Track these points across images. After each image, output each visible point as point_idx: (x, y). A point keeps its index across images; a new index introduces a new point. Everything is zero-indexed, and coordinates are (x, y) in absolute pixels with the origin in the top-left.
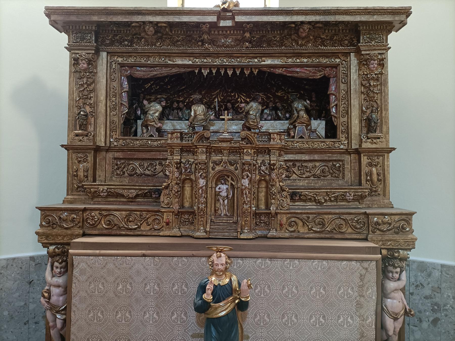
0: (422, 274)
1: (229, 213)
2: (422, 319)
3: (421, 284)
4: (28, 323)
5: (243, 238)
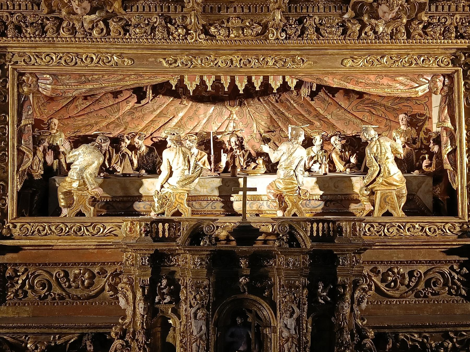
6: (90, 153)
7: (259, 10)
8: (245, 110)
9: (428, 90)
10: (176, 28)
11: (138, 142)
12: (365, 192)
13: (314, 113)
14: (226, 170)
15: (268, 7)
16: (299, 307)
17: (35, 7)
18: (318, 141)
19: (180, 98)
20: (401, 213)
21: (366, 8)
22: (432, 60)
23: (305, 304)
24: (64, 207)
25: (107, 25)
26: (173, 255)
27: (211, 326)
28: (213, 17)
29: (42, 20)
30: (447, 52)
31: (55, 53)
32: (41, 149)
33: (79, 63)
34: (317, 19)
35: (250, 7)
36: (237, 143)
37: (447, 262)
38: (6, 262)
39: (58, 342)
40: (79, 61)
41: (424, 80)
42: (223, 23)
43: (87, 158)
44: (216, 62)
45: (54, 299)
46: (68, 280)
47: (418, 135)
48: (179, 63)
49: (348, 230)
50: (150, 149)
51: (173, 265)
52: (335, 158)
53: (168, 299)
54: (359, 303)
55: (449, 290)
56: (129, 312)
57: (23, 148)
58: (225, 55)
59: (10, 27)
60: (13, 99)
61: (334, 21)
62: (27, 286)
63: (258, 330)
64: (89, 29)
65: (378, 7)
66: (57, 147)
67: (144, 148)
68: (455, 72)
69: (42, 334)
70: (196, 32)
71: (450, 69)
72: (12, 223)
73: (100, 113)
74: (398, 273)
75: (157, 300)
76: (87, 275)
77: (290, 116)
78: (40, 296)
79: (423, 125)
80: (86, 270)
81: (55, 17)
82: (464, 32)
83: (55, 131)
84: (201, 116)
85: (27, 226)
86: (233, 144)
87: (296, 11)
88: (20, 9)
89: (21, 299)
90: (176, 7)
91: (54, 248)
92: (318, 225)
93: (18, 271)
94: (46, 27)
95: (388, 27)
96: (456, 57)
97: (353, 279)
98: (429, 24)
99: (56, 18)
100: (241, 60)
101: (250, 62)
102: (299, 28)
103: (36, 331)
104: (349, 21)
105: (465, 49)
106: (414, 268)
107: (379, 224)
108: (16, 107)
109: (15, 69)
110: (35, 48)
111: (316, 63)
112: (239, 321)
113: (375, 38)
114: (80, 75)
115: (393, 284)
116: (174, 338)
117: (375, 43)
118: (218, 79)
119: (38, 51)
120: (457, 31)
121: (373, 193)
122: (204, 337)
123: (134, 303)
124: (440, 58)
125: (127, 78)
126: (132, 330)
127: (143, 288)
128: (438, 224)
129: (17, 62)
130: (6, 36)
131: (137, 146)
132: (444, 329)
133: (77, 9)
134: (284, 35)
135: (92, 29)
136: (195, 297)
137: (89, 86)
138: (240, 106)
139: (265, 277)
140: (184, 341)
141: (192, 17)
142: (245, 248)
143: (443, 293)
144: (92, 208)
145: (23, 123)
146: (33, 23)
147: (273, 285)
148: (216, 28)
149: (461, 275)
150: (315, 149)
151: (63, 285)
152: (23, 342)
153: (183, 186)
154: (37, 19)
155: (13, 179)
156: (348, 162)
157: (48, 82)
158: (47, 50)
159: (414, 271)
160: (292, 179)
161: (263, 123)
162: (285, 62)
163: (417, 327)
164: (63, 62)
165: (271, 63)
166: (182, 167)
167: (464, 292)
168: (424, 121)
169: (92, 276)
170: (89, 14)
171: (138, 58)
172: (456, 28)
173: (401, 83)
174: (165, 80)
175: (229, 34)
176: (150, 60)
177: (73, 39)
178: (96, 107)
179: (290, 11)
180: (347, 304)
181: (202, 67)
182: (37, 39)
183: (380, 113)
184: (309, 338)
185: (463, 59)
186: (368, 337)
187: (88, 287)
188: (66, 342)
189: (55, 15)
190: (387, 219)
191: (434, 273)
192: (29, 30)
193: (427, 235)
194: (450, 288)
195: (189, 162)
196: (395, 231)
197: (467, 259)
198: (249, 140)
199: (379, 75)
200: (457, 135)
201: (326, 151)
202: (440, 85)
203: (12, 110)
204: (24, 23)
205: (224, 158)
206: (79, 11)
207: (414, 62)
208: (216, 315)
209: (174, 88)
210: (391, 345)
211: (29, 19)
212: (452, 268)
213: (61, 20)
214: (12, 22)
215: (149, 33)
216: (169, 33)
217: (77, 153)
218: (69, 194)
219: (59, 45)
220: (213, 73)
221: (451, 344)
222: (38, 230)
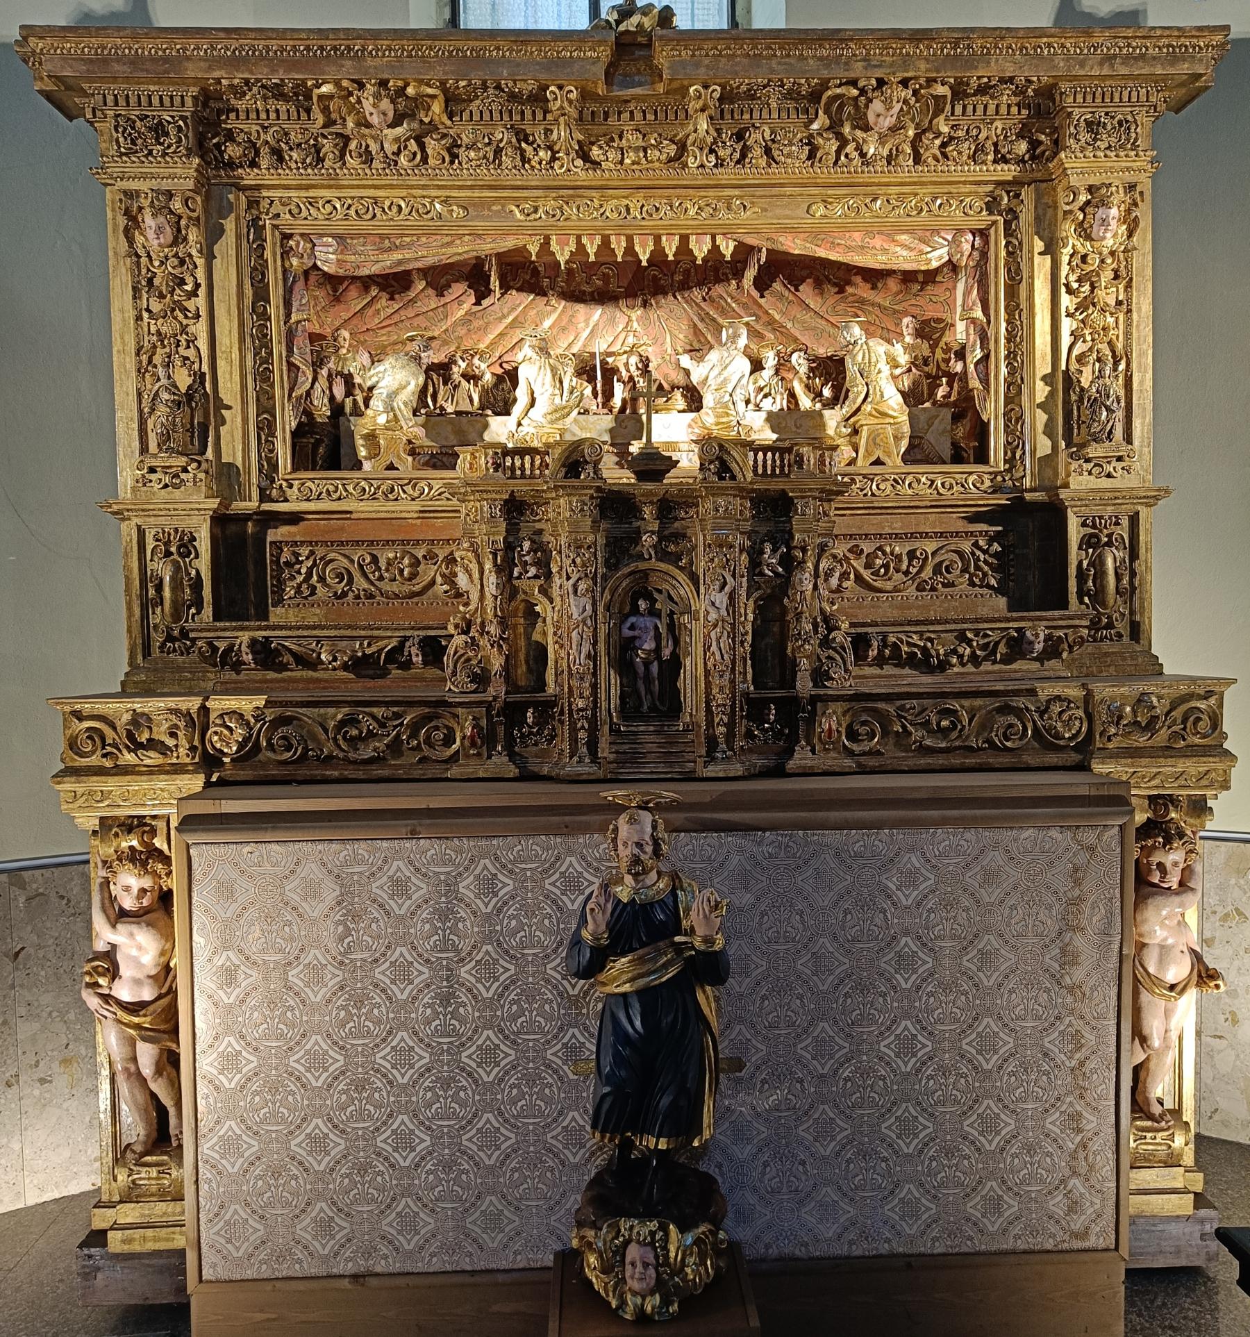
0: (1242, 882)
1: (662, 704)
2: (1240, 1016)
3: (1237, 909)
4: (18, 1082)
5: (713, 775)
6: (403, 367)
7: (671, 116)
8: (653, 314)
9: (947, 258)
10: (535, 149)
11: (480, 365)
12: (844, 430)
13: (765, 318)
14: (622, 410)
15: (687, 111)
16: (734, 576)
17: (304, 115)
18: (770, 360)
19: (545, 295)
20: (899, 461)
21: (849, 109)
22: (954, 203)
23: (743, 576)
24: (366, 458)
25: (422, 146)
26: (539, 506)
27: (600, 609)
28: (596, 130)
29: (316, 140)
30: (980, 190)
31: (339, 199)
32: (324, 372)
33: (378, 215)
34: (767, 133)
35: (656, 111)
36: (640, 366)
38: (280, 539)
39: (368, 651)
40: (378, 212)
41: (941, 240)
42: (612, 140)
43: (398, 377)
44: (602, 210)
45: (358, 597)
46: (379, 569)
47: (934, 353)
49: (812, 462)
50: (499, 379)
51: (539, 521)
52: (799, 389)
53: (533, 571)
54: (828, 576)
55: (970, 579)
56: (474, 596)
57: (296, 360)
58: (617, 198)
59: (265, 151)
60: (276, 278)
61: (794, 136)
62: (315, 578)
63: (672, 619)
64: (393, 153)
65: (867, 106)
66: (350, 375)
67: (488, 377)
68: (991, 225)
69: (342, 638)
70: (568, 154)
72: (286, 480)
73: (416, 322)
74: (892, 554)
75: (516, 574)
76: (406, 561)
78: (336, 593)
79: (941, 336)
80: (405, 553)
81: (337, 134)
82: (1009, 152)
83: (344, 351)
84: (580, 326)
85: (309, 484)
86: (633, 369)
87: (733, 118)
88: (278, 118)
89: (306, 598)
90: (534, 112)
91: (353, 516)
92: (765, 455)
93: (300, 555)
94: (323, 151)
95: (883, 144)
96: (995, 199)
97: (818, 541)
98: (951, 138)
99: (339, 135)
100: (643, 206)
101: (657, 209)
102: (739, 147)
103: (333, 633)
104: (820, 135)
105: (1008, 183)
106: (917, 545)
107: (865, 476)
108: (281, 291)
109: (275, 227)
110: (308, 188)
111: (766, 210)
112: (642, 604)
113: (863, 164)
114: (382, 237)
115: (882, 570)
116: (545, 634)
117: (863, 172)
118: (606, 242)
120: (996, 151)
121: (856, 432)
122: (589, 622)
123: (481, 579)
124: (968, 200)
125: (458, 242)
126: (479, 620)
127: (495, 555)
128: (957, 476)
129: (278, 215)
130: (259, 167)
131: (477, 371)
132: (959, 627)
133: (371, 114)
134: (712, 158)
135: (398, 153)
136: (574, 561)
137: (397, 256)
138: (645, 307)
139: (680, 536)
140: (559, 633)
141: (562, 127)
142: (649, 486)
143: (961, 584)
144: (410, 459)
145: (294, 318)
146: (300, 144)
147: (694, 548)
148: (601, 147)
149: (991, 556)
150: (767, 373)
151: (371, 576)
152: (313, 651)
153: (552, 422)
154: (307, 137)
155: (283, 409)
156: (820, 394)
157: (331, 250)
158: (326, 193)
159: (915, 550)
160: (726, 407)
161: (681, 336)
162: (715, 210)
163: (918, 623)
164: (352, 212)
165: (692, 212)
166: (551, 390)
167: (993, 582)
168: (943, 330)
169: (416, 563)
170: (392, 126)
171: (474, 205)
172: (996, 145)
173: (903, 246)
174: (520, 243)
175: (623, 159)
176: (494, 208)
177: (368, 171)
178: (410, 312)
179: (722, 118)
180: (807, 575)
181: (580, 220)
182: (309, 171)
184: (749, 628)
185: (1006, 199)
186: (839, 629)
187: (410, 579)
188: (380, 651)
189: (337, 128)
190: (877, 469)
191: (948, 552)
192: (295, 155)
193: (938, 493)
194: (971, 576)
195: (561, 382)
196: (889, 488)
197: (1000, 528)
198: (659, 365)
199: (869, 232)
200: (991, 332)
201: (783, 379)
202: (967, 247)
203: (276, 296)
204: (287, 143)
205: (619, 392)
206: (375, 120)
207: (925, 208)
208: (607, 596)
209: (534, 258)
210: (876, 652)
211: (295, 138)
212: (976, 545)
213: (347, 139)
214: (267, 142)
215: (491, 159)
216: (524, 160)
217: (381, 368)
218: (371, 437)
219: (345, 183)
220: (595, 228)
221: (968, 650)
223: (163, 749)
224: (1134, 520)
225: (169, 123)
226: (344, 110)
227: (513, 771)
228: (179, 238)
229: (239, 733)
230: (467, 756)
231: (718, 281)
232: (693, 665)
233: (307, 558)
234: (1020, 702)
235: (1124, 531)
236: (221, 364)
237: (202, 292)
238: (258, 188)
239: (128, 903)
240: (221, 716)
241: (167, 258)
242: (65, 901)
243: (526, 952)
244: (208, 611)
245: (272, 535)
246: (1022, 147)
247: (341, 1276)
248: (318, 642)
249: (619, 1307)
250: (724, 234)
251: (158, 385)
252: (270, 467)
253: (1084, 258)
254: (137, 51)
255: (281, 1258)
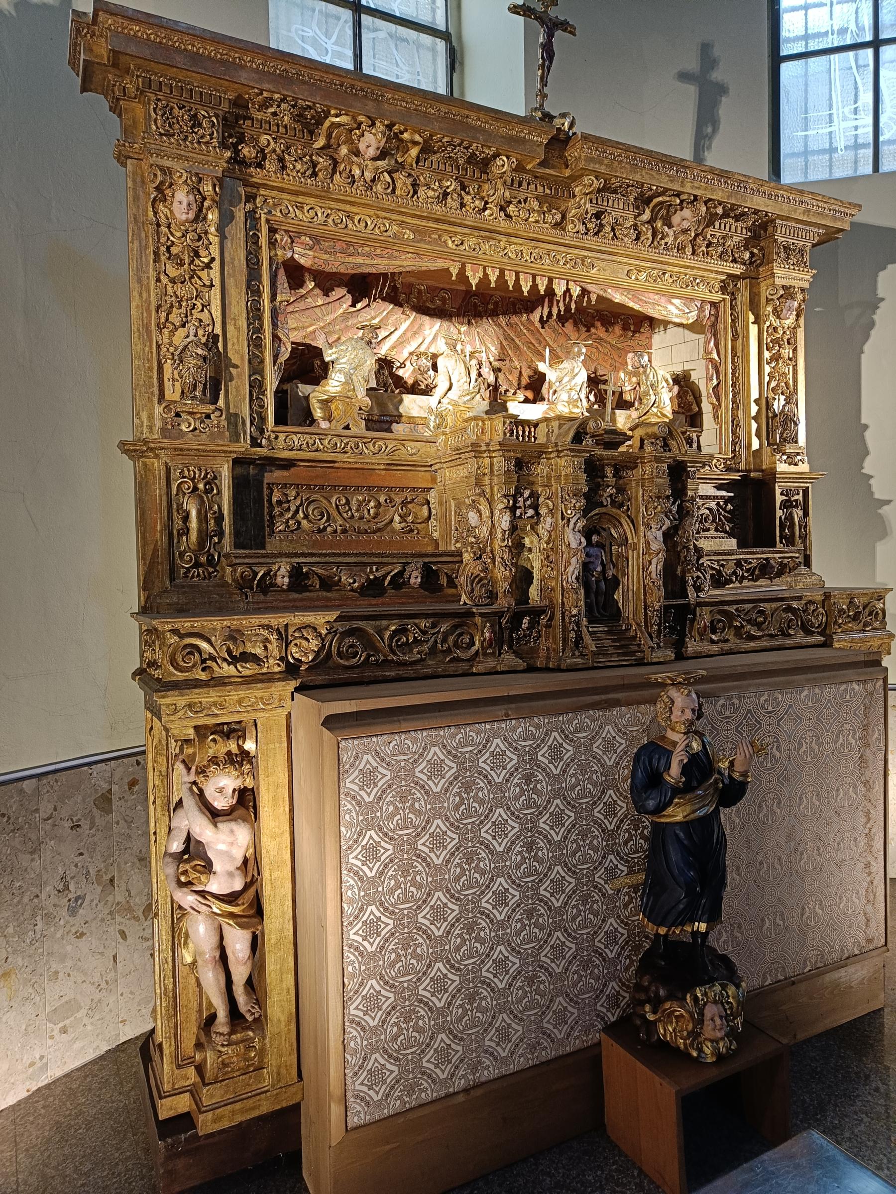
8: (474, 331)
19: (401, 306)
37: (715, 497)
39: (378, 574)
46: (350, 509)
48: (466, 246)
71: (717, 297)
76: (372, 504)
77: (520, 344)
91: (336, 465)
119: (299, 200)
164: (330, 221)
174: (446, 266)
176: (433, 236)
183: (606, 351)
188: (385, 577)
197: (732, 494)
200: (722, 369)
216: (462, 205)
222: (307, 443)
223: (255, 659)
224: (806, 492)
225: (204, 117)
226: (343, 138)
227: (521, 664)
228: (200, 217)
229: (314, 644)
230: (485, 654)
231: (515, 313)
232: (632, 581)
233: (295, 498)
234: (795, 605)
235: (800, 497)
236: (230, 328)
237: (216, 265)
238: (258, 186)
239: (220, 803)
240: (299, 629)
241: (187, 231)
242: (5, 819)
243: (581, 801)
244: (227, 541)
245: (268, 477)
246: (747, 255)
247: (458, 1093)
248: (338, 567)
249: (699, 1055)
250: (575, 281)
251: (188, 340)
252: (259, 420)
253: (775, 329)
254: (210, 53)
255: (410, 1090)
